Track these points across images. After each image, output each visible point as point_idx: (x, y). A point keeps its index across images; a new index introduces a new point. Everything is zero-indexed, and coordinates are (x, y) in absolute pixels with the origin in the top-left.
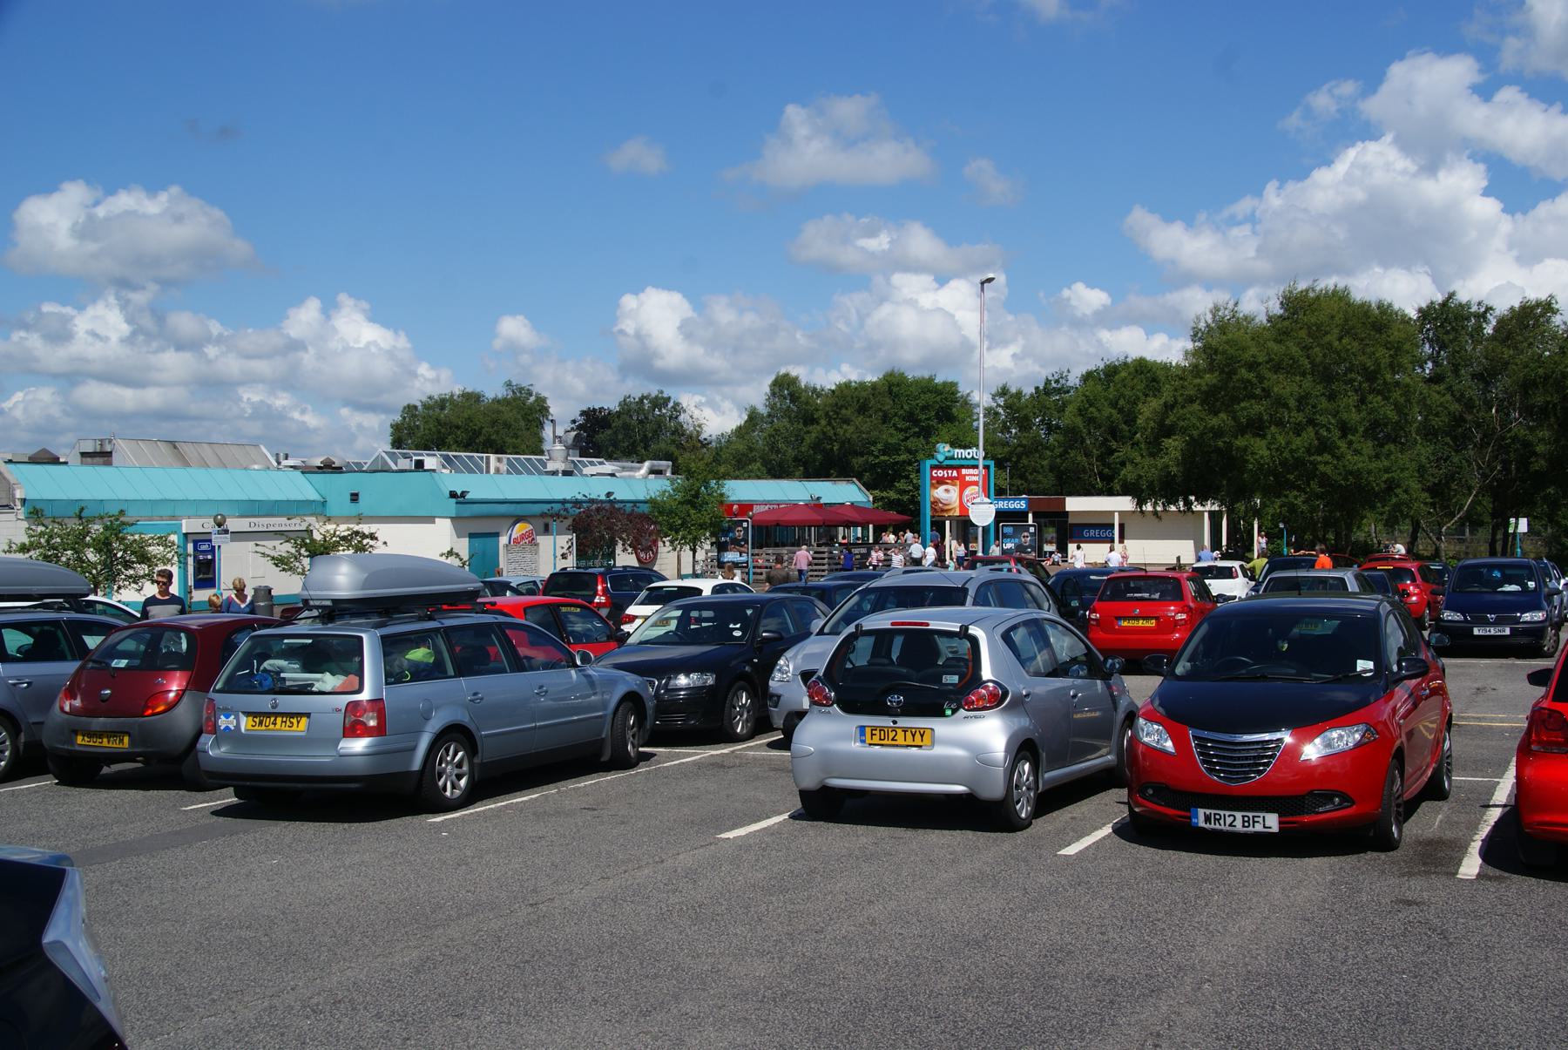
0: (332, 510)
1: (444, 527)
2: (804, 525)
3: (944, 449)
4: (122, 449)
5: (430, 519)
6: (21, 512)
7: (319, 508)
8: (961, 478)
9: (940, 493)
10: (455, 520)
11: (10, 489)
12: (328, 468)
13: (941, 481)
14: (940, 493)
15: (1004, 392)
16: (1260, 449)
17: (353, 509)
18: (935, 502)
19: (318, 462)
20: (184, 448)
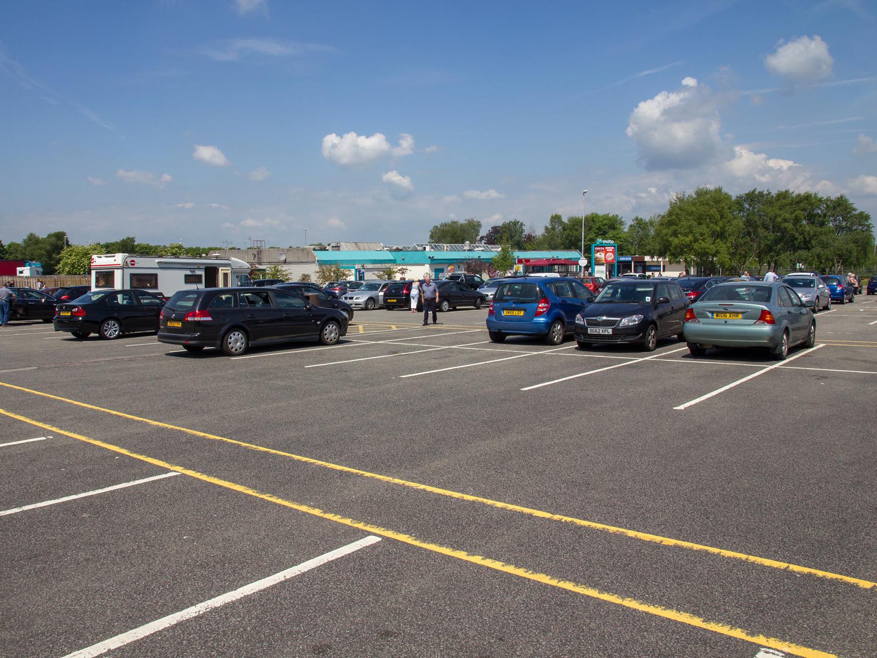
0: (398, 262)
1: (427, 266)
2: (546, 266)
3: (599, 240)
4: (343, 245)
5: (423, 265)
6: (678, 287)
7: (393, 262)
8: (605, 250)
9: (598, 255)
10: (430, 265)
11: (315, 257)
12: (398, 250)
13: (598, 251)
14: (598, 255)
15: (637, 219)
16: (675, 241)
17: (402, 262)
18: (596, 258)
19: (395, 248)
20: (359, 244)
